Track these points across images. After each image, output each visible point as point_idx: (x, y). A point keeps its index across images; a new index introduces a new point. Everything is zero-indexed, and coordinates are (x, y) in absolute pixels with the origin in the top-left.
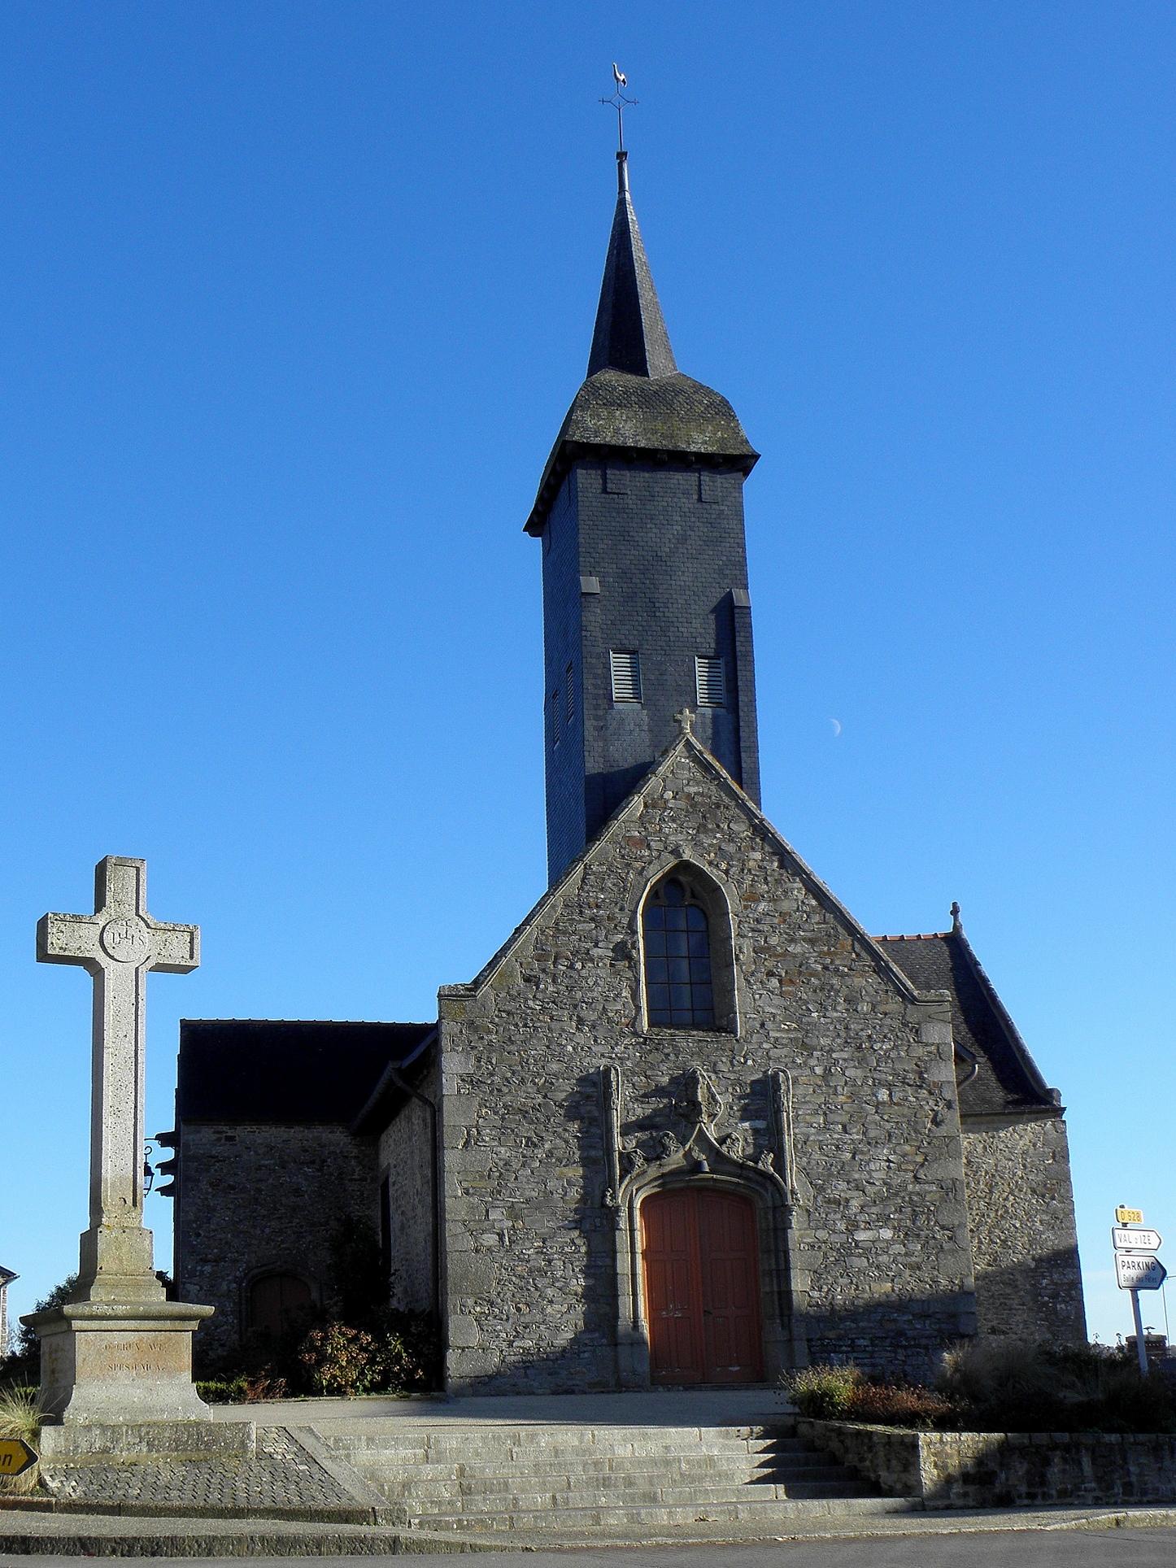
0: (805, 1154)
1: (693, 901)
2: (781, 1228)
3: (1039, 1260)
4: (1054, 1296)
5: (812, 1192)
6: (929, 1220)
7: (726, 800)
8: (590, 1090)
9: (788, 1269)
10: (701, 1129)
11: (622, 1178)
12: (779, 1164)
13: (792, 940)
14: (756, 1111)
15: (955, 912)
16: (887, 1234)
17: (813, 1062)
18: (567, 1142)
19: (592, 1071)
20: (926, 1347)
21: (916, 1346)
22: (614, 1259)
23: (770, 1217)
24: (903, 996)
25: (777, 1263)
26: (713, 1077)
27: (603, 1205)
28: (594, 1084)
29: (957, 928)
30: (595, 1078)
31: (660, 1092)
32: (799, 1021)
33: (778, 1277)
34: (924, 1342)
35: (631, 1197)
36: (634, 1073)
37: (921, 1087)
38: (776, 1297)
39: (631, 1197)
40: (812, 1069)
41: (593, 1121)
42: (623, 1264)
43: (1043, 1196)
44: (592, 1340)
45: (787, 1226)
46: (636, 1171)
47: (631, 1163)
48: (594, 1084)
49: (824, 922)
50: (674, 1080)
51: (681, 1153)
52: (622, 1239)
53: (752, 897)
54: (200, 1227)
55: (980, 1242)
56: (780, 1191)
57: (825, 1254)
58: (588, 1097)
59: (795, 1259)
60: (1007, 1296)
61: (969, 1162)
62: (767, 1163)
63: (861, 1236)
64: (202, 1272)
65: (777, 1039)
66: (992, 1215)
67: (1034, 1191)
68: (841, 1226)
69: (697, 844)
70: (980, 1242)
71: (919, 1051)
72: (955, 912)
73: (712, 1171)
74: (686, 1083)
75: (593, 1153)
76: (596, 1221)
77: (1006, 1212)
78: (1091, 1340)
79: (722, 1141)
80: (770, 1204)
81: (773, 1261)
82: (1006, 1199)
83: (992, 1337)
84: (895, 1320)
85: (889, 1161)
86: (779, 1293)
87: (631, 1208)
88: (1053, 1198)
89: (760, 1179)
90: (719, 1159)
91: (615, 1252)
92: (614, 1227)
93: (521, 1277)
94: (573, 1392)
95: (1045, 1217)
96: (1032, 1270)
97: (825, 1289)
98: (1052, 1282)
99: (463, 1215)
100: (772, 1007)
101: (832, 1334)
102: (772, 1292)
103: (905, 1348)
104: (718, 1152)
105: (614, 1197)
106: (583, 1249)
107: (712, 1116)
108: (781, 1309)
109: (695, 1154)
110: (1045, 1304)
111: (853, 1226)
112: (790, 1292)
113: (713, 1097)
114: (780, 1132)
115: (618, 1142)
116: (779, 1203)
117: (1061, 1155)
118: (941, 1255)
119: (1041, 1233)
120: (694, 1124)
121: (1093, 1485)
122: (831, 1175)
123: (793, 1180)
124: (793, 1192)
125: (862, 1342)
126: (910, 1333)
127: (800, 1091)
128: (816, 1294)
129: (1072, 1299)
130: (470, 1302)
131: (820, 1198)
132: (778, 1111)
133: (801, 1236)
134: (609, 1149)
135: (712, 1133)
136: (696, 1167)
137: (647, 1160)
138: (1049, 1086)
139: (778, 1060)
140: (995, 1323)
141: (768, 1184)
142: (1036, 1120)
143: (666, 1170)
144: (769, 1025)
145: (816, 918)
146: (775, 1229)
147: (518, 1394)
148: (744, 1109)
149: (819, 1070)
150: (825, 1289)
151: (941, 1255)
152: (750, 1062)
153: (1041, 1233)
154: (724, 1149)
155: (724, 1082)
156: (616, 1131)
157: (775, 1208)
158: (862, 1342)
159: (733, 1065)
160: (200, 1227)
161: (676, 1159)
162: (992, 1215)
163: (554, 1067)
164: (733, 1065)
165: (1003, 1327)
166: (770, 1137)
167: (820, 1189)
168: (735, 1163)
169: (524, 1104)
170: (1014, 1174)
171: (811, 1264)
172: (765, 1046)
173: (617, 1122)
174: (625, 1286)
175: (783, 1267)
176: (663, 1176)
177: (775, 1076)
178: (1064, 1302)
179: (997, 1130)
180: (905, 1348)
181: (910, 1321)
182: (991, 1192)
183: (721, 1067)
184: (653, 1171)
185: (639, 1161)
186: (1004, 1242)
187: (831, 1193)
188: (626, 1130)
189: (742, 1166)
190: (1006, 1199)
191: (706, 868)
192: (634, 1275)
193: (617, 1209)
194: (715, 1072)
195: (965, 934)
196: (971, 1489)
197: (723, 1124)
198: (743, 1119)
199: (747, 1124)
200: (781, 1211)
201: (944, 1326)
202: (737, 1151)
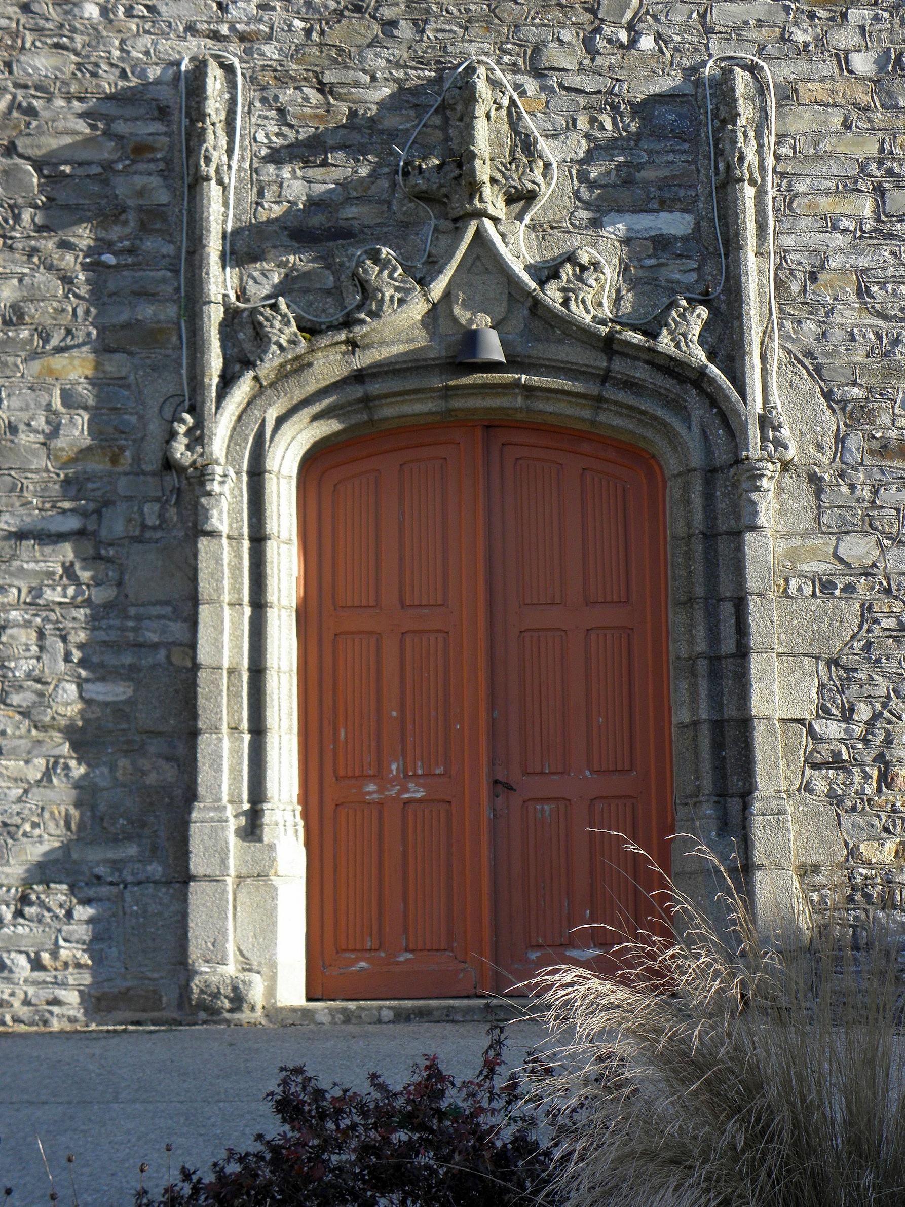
0: (812, 308)
2: (724, 530)
5: (831, 422)
8: (148, 129)
9: (743, 653)
10: (480, 236)
11: (227, 381)
12: (726, 340)
14: (664, 184)
17: (845, 38)
18: (67, 280)
19: (153, 73)
22: (193, 623)
23: (697, 500)
25: (714, 636)
26: (531, 86)
27: (169, 465)
28: (163, 113)
30: (165, 94)
31: (359, 134)
33: (715, 675)
35: (257, 457)
36: (283, 78)
38: (705, 742)
39: (257, 457)
40: (843, 59)
41: (152, 219)
42: (222, 639)
44: (116, 865)
45: (743, 522)
46: (268, 366)
47: (260, 338)
48: (163, 113)
50: (406, 98)
51: (417, 308)
52: (222, 565)
56: (729, 423)
57: (867, 608)
58: (141, 150)
59: (767, 620)
62: (687, 335)
73: (514, 363)
74: (445, 103)
75: (147, 312)
76: (133, 520)
79: (546, 273)
80: (696, 459)
81: (700, 632)
86: (718, 726)
87: (257, 475)
89: (666, 383)
90: (535, 320)
91: (194, 600)
92: (196, 528)
97: (864, 712)
102: (695, 724)
104: (536, 306)
105: (198, 437)
107: (522, 199)
108: (720, 769)
109: (462, 314)
112: (745, 723)
113: (527, 146)
114: (731, 244)
115: (220, 282)
116: (722, 456)
120: (459, 221)
123: (771, 388)
124: (765, 422)
127: (802, 122)
128: (833, 729)
131: (854, 442)
132: (727, 183)
133: (793, 555)
134: (193, 299)
135: (518, 250)
136: (463, 354)
137: (310, 330)
139: (736, 33)
141: (692, 398)
143: (361, 360)
146: (710, 536)
150: (864, 712)
152: (647, 43)
154: (552, 295)
155: (562, 100)
156: (214, 247)
157: (711, 473)
159: (592, 51)
161: (400, 324)
163: (41, 63)
164: (592, 51)
166: (698, 260)
168: (584, 336)
173: (219, 214)
174: (222, 707)
175: (728, 646)
176: (359, 377)
177: (722, 87)
183: (554, 55)
184: (330, 364)
185: (283, 331)
188: (243, 249)
189: (609, 345)
192: (258, 671)
193: (199, 476)
194: (538, 73)
197: (545, 228)
200: (727, 480)
202: (598, 298)
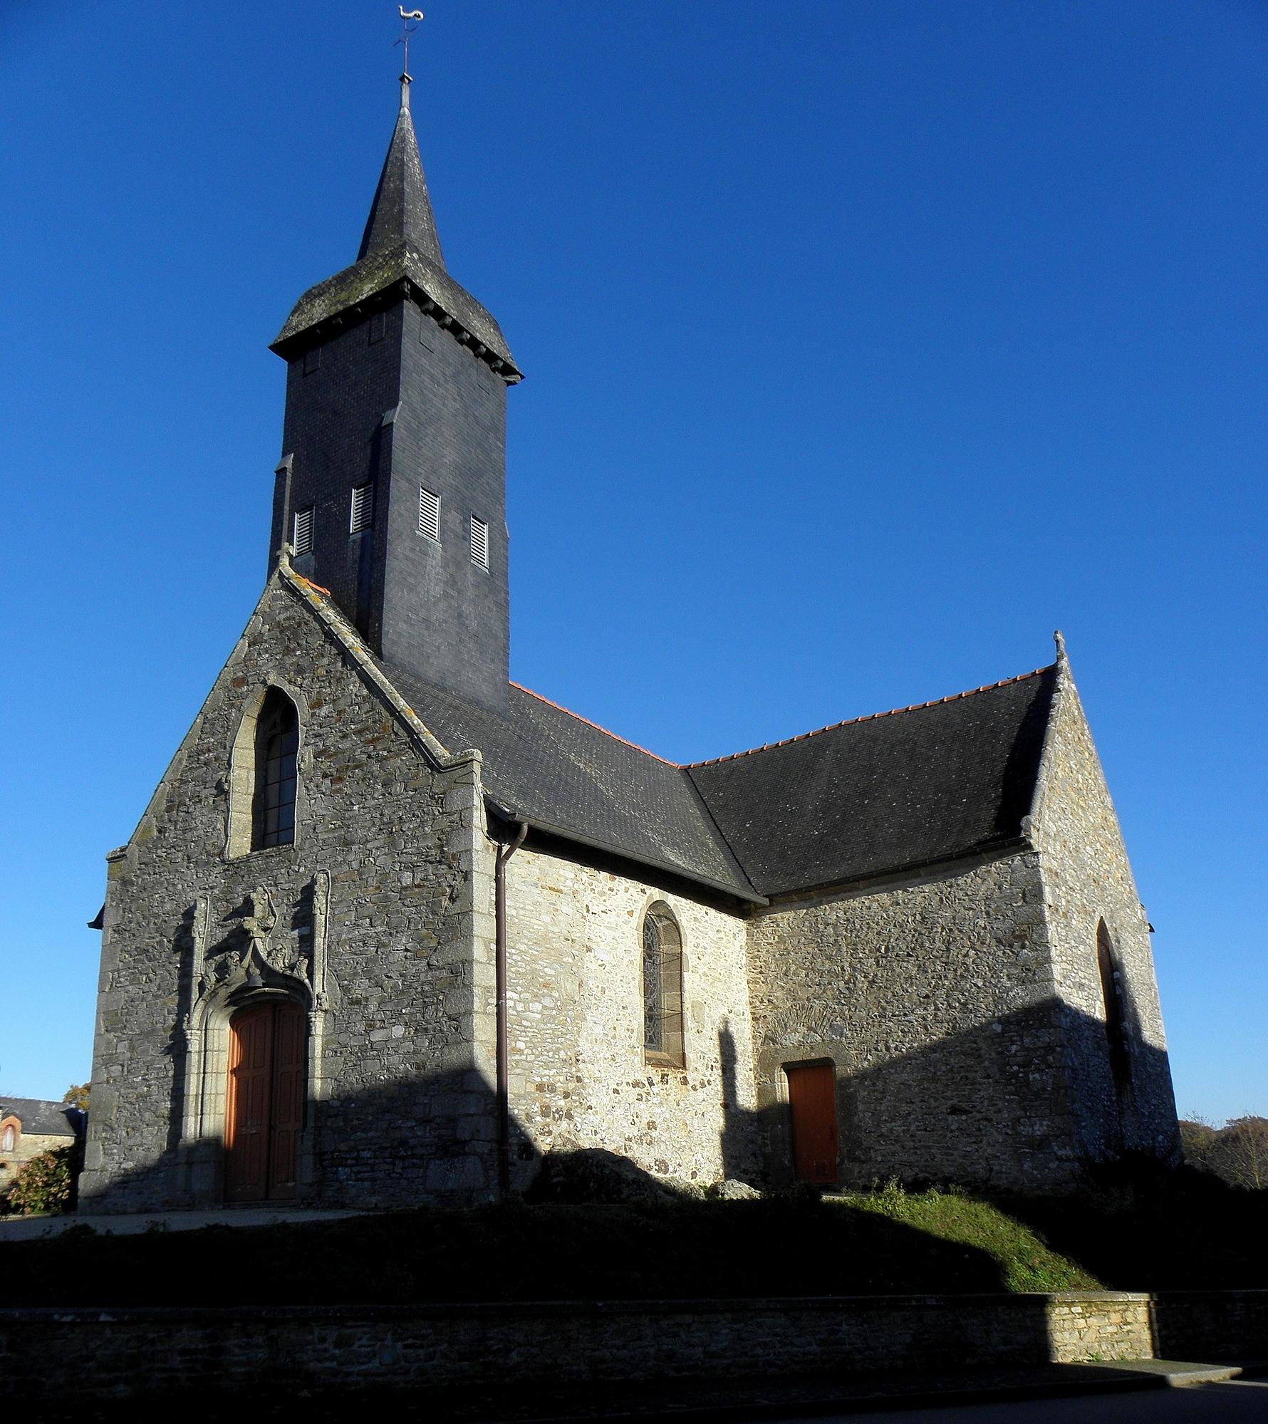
3: (1005, 1021)
4: (1026, 1065)
6: (437, 1010)
7: (306, 615)
13: (344, 737)
16: (398, 1031)
20: (421, 1157)
21: (413, 1156)
24: (432, 767)
32: (343, 819)
34: (419, 1151)
36: (219, 900)
37: (440, 862)
40: (350, 864)
43: (1011, 946)
49: (373, 709)
53: (317, 704)
55: (937, 1009)
61: (923, 918)
63: (377, 1036)
65: (324, 840)
66: (950, 976)
67: (999, 942)
68: (360, 1028)
69: (281, 668)
70: (937, 1009)
71: (444, 822)
73: (265, 985)
77: (967, 970)
78: (1181, 1116)
82: (966, 955)
83: (950, 1118)
84: (399, 1128)
85: (407, 950)
88: (1023, 947)
93: (131, 1103)
95: (1013, 971)
96: (997, 1035)
101: (343, 1146)
103: (403, 1158)
106: (171, 1073)
111: (370, 1027)
117: (1034, 894)
118: (446, 1050)
119: (1008, 990)
122: (356, 974)
125: (366, 1154)
126: (412, 1142)
130: (101, 1128)
140: (955, 1101)
142: (1000, 857)
143: (233, 989)
144: (320, 828)
145: (367, 707)
148: (294, 918)
149: (355, 865)
151: (446, 1050)
153: (1008, 990)
158: (366, 1154)
162: (950, 976)
165: (964, 1105)
167: (345, 990)
169: (147, 945)
170: (975, 925)
171: (333, 1072)
176: (232, 994)
178: (1039, 1071)
179: (955, 876)
180: (403, 1158)
181: (412, 1128)
182: (948, 950)
186: (965, 1005)
187: (357, 993)
190: (966, 955)
198: (293, 929)
199: (296, 932)
201: (443, 1132)
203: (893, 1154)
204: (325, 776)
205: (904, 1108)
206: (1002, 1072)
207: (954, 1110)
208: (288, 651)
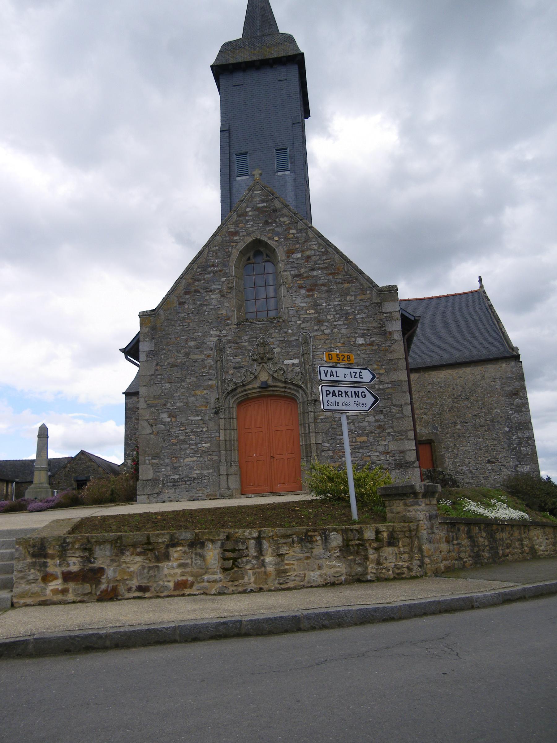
1: (268, 258)
4: (520, 444)
14: (294, 354)
15: (480, 280)
25: (305, 430)
29: (482, 286)
53: (290, 252)
54: (132, 436)
60: (495, 445)
64: (133, 454)
72: (480, 280)
84: (370, 456)
94: (198, 500)
98: (518, 437)
99: (147, 417)
100: (301, 302)
108: (307, 452)
110: (515, 448)
121: (219, 576)
129: (529, 445)
138: (514, 346)
140: (489, 458)
147: (171, 501)
160: (132, 436)
172: (299, 322)
191: (269, 242)
195: (485, 288)
196: (71, 586)
203: (463, 479)
204: (301, 287)
205: (467, 461)
206: (509, 446)
207: (489, 462)
208: (266, 223)
